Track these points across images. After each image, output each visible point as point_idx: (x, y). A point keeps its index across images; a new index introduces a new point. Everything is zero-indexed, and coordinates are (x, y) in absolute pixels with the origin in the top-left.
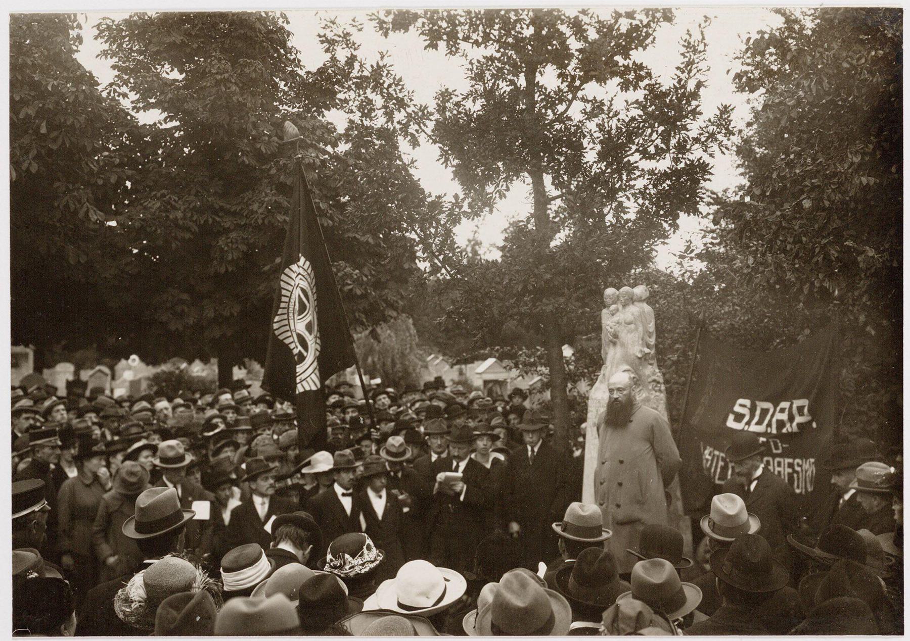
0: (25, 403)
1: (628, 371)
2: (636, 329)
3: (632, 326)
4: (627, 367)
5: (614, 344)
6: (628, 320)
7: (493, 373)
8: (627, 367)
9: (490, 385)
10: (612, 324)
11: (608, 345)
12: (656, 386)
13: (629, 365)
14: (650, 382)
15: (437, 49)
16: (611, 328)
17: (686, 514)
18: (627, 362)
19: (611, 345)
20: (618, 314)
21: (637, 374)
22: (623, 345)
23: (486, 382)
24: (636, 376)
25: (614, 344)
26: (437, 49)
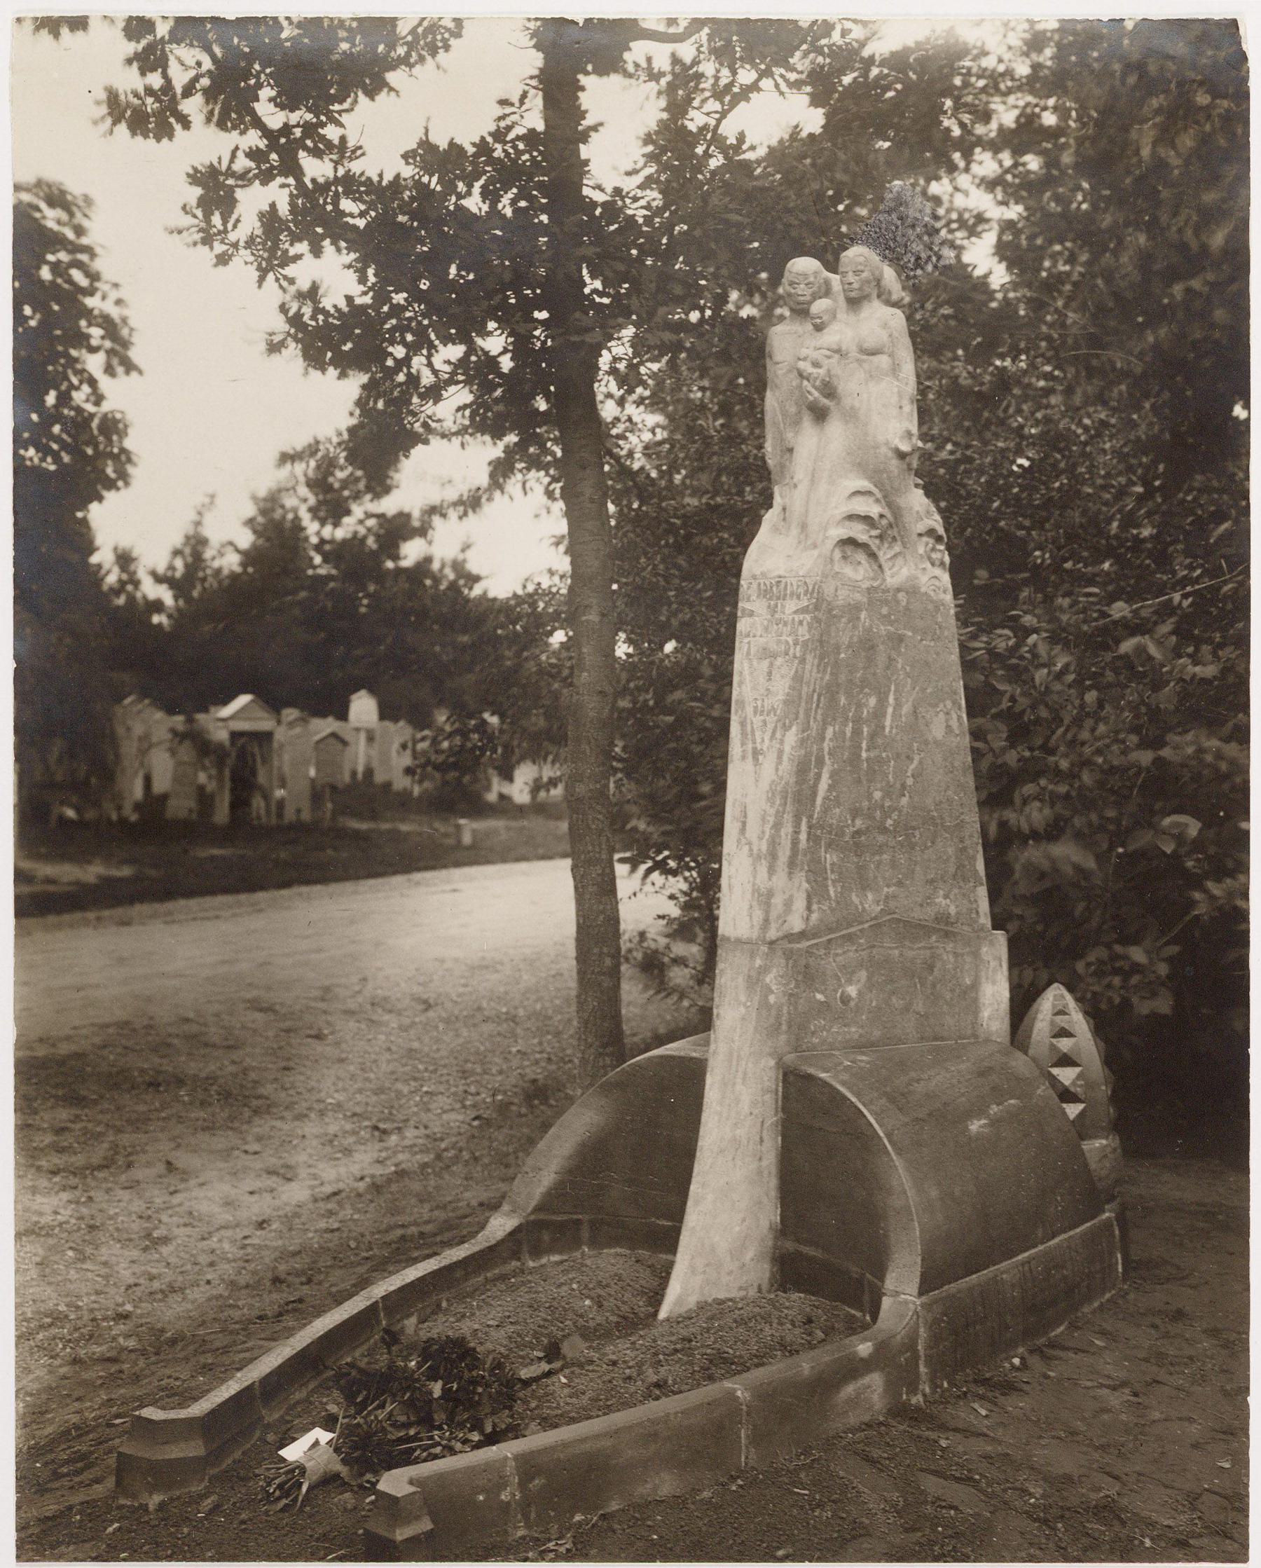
0: (719, 762)
1: (869, 493)
2: (895, 369)
3: (883, 361)
4: (864, 484)
5: (820, 415)
6: (870, 343)
7: (249, 719)
8: (864, 484)
9: (243, 740)
10: (816, 355)
11: (796, 423)
12: (933, 549)
13: (870, 479)
14: (920, 535)
15: (216, 265)
16: (816, 364)
17: (996, 926)
18: (862, 467)
19: (807, 422)
20: (835, 327)
21: (890, 505)
22: (851, 416)
23: (235, 735)
24: (887, 512)
25: (820, 415)
26: (216, 265)
